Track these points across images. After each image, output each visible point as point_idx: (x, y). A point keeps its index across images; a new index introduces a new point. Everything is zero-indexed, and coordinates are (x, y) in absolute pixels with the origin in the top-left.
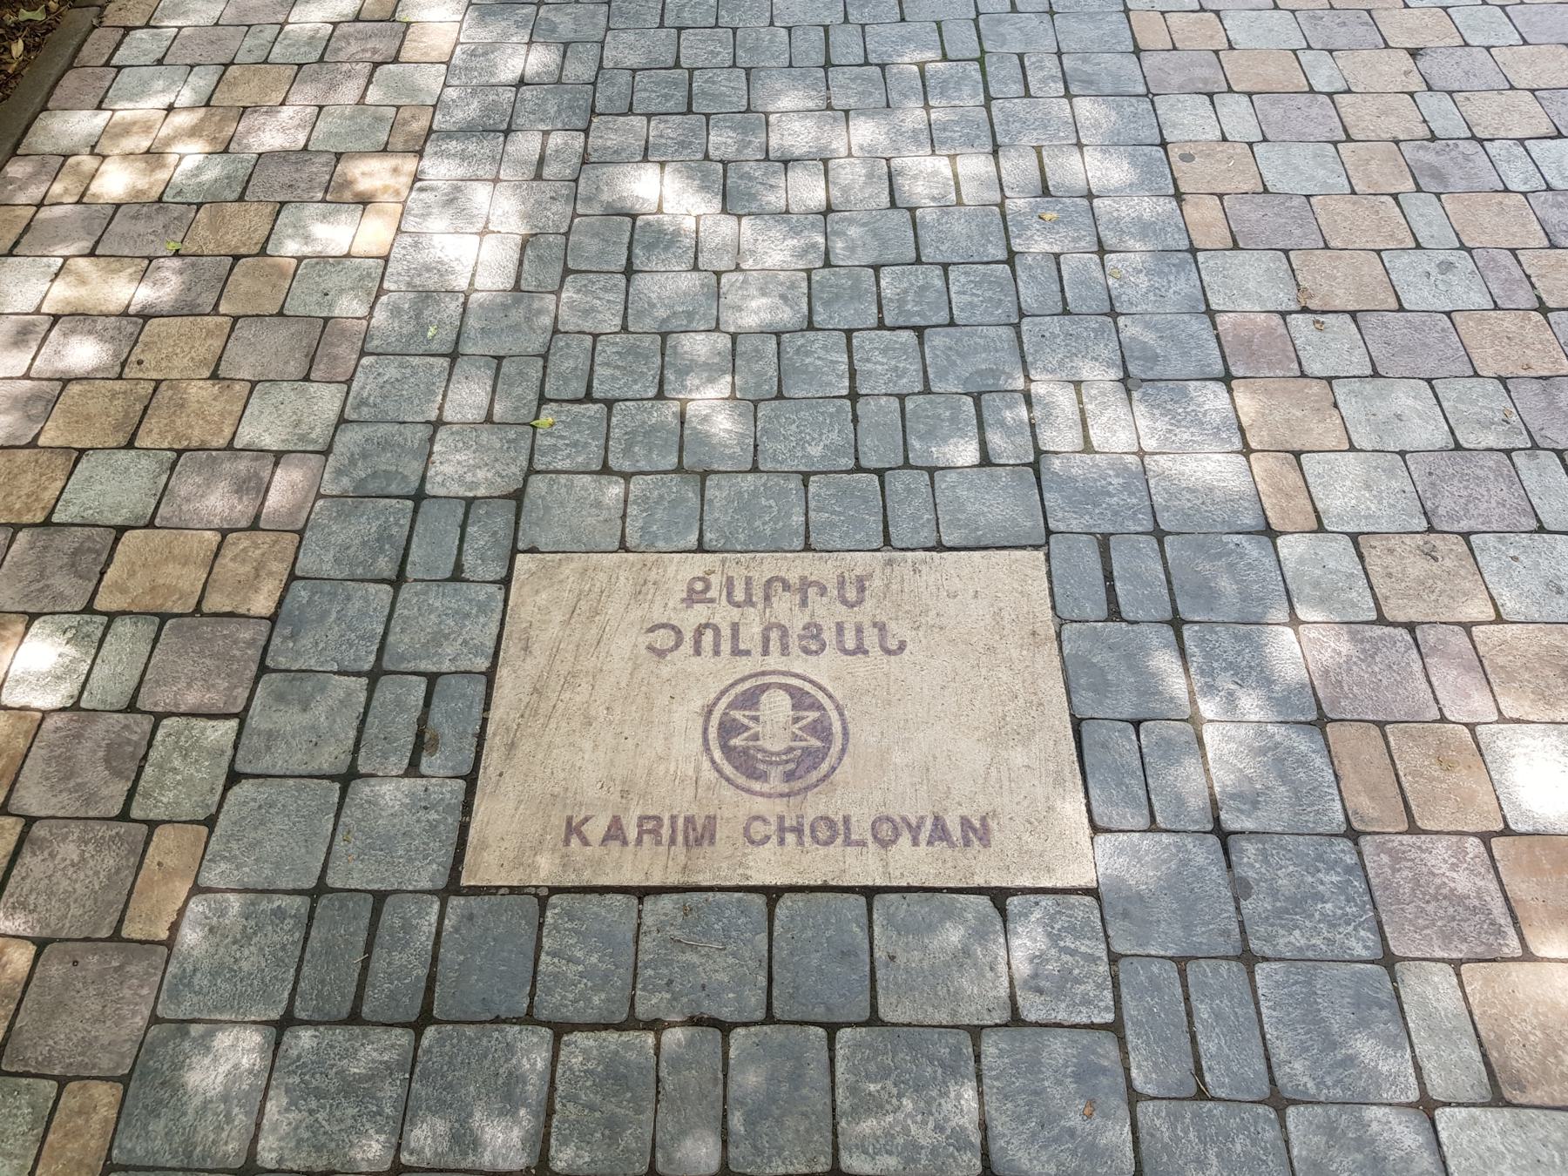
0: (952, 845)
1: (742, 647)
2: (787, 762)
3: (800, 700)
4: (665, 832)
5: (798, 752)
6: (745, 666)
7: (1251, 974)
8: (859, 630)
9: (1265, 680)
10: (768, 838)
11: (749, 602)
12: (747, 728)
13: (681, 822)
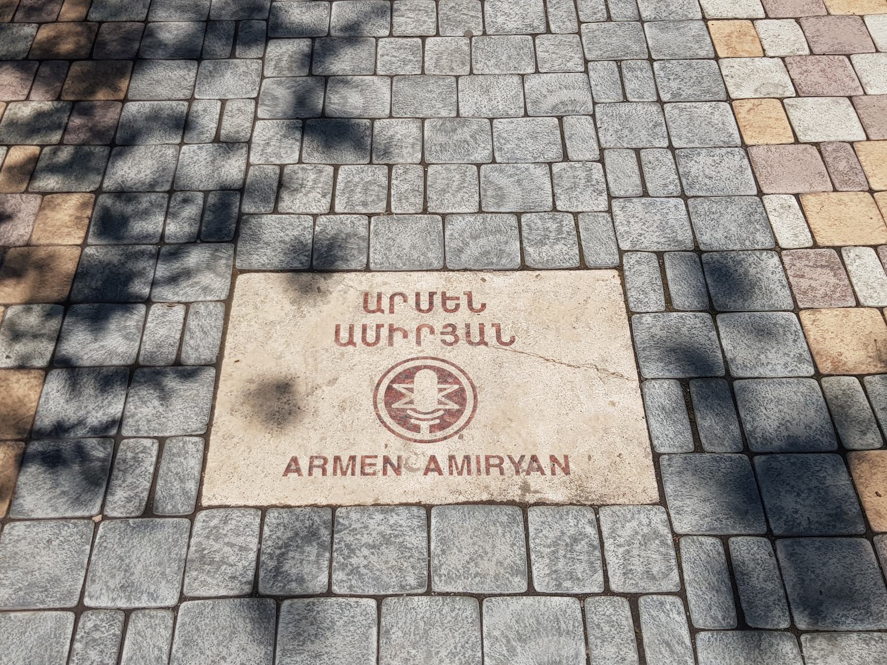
0: (440, 473)
2: (435, 418)
3: (444, 376)
5: (441, 413)
7: (652, 65)
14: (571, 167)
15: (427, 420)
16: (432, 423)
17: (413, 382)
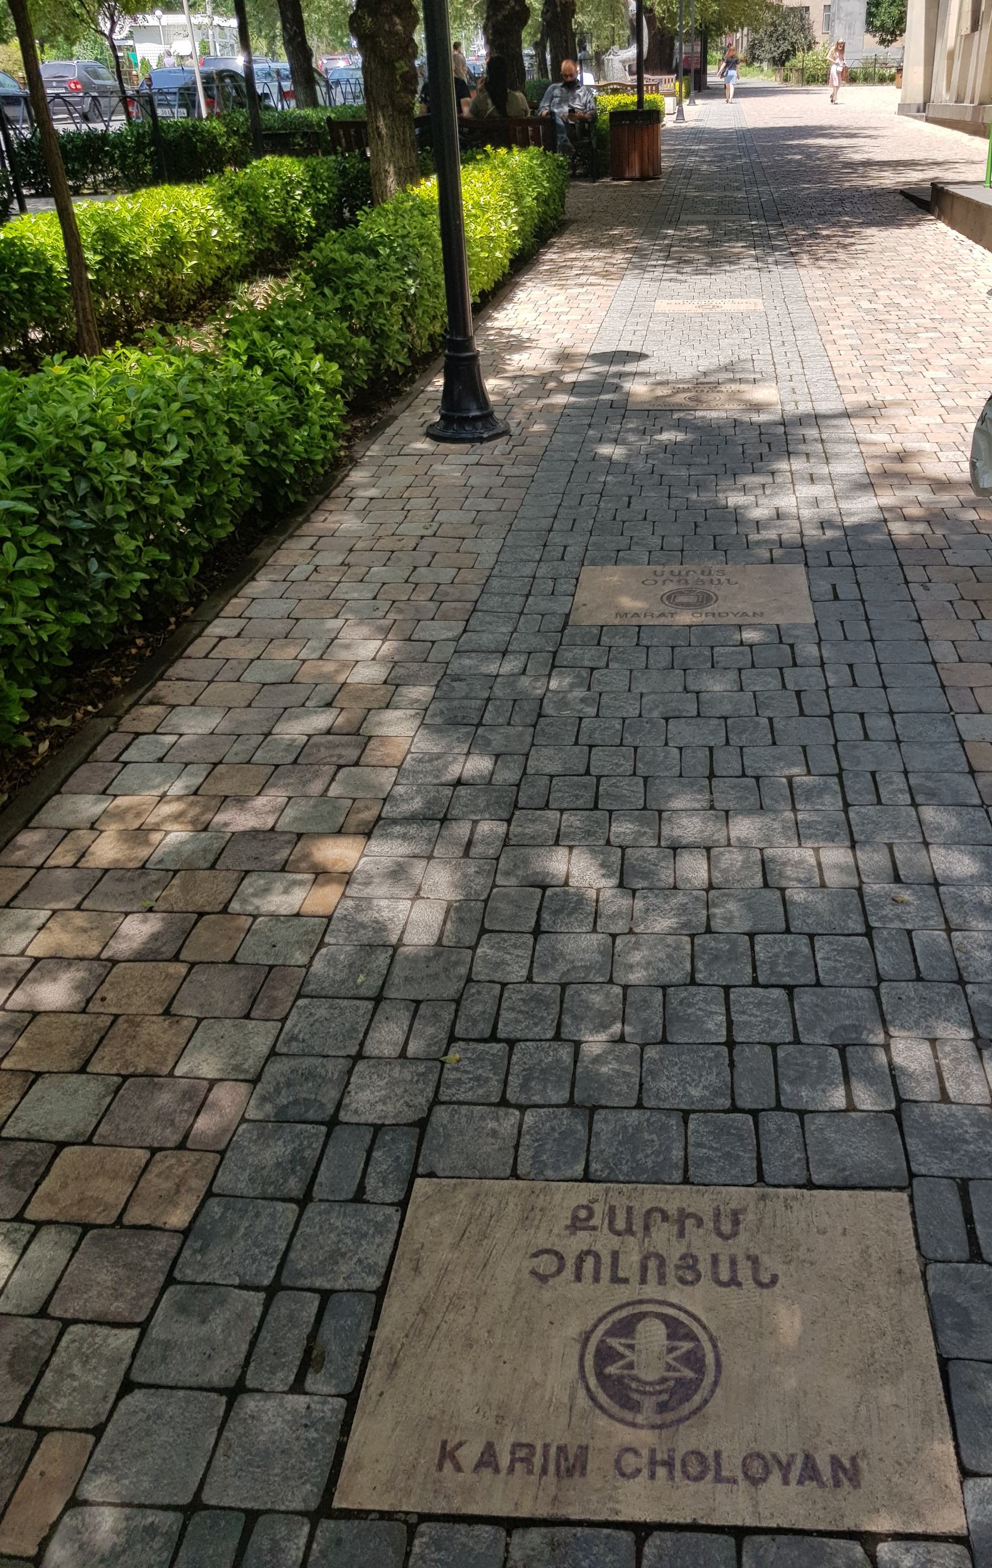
0: (822, 1485)
1: (621, 1274)
2: (660, 1392)
3: (675, 1329)
4: (538, 1461)
6: (624, 1293)
8: (733, 1262)
10: (639, 1471)
11: (629, 1231)
12: (623, 1357)
13: (553, 1450)
14: (801, 1051)
15: (651, 1394)
17: (633, 1338)
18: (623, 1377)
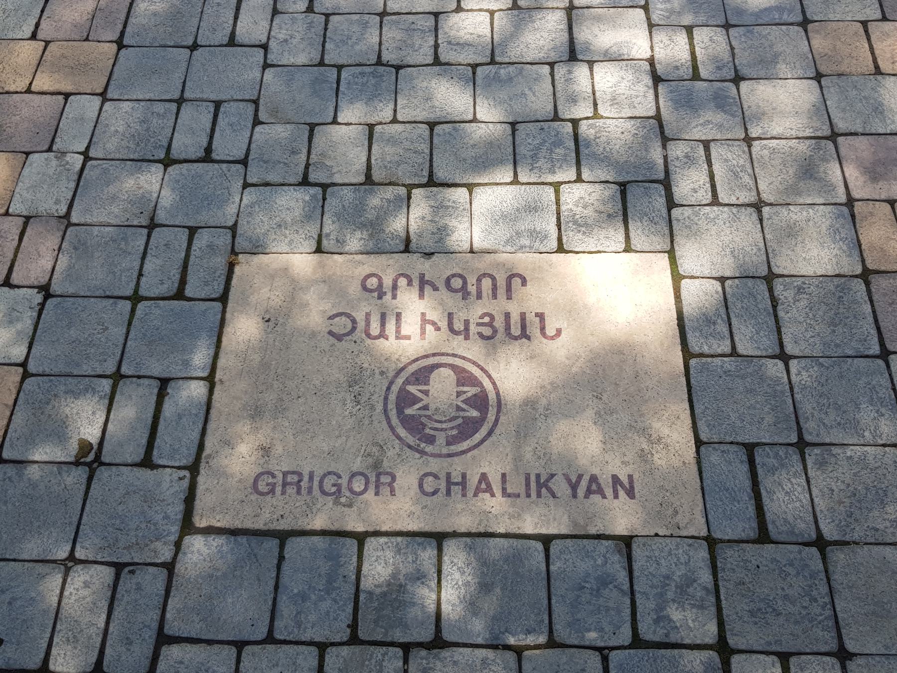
0: (493, 495)
2: (452, 428)
4: (304, 484)
5: (460, 421)
9: (580, 151)
13: (533, 478)
16: (450, 433)
18: (420, 416)
